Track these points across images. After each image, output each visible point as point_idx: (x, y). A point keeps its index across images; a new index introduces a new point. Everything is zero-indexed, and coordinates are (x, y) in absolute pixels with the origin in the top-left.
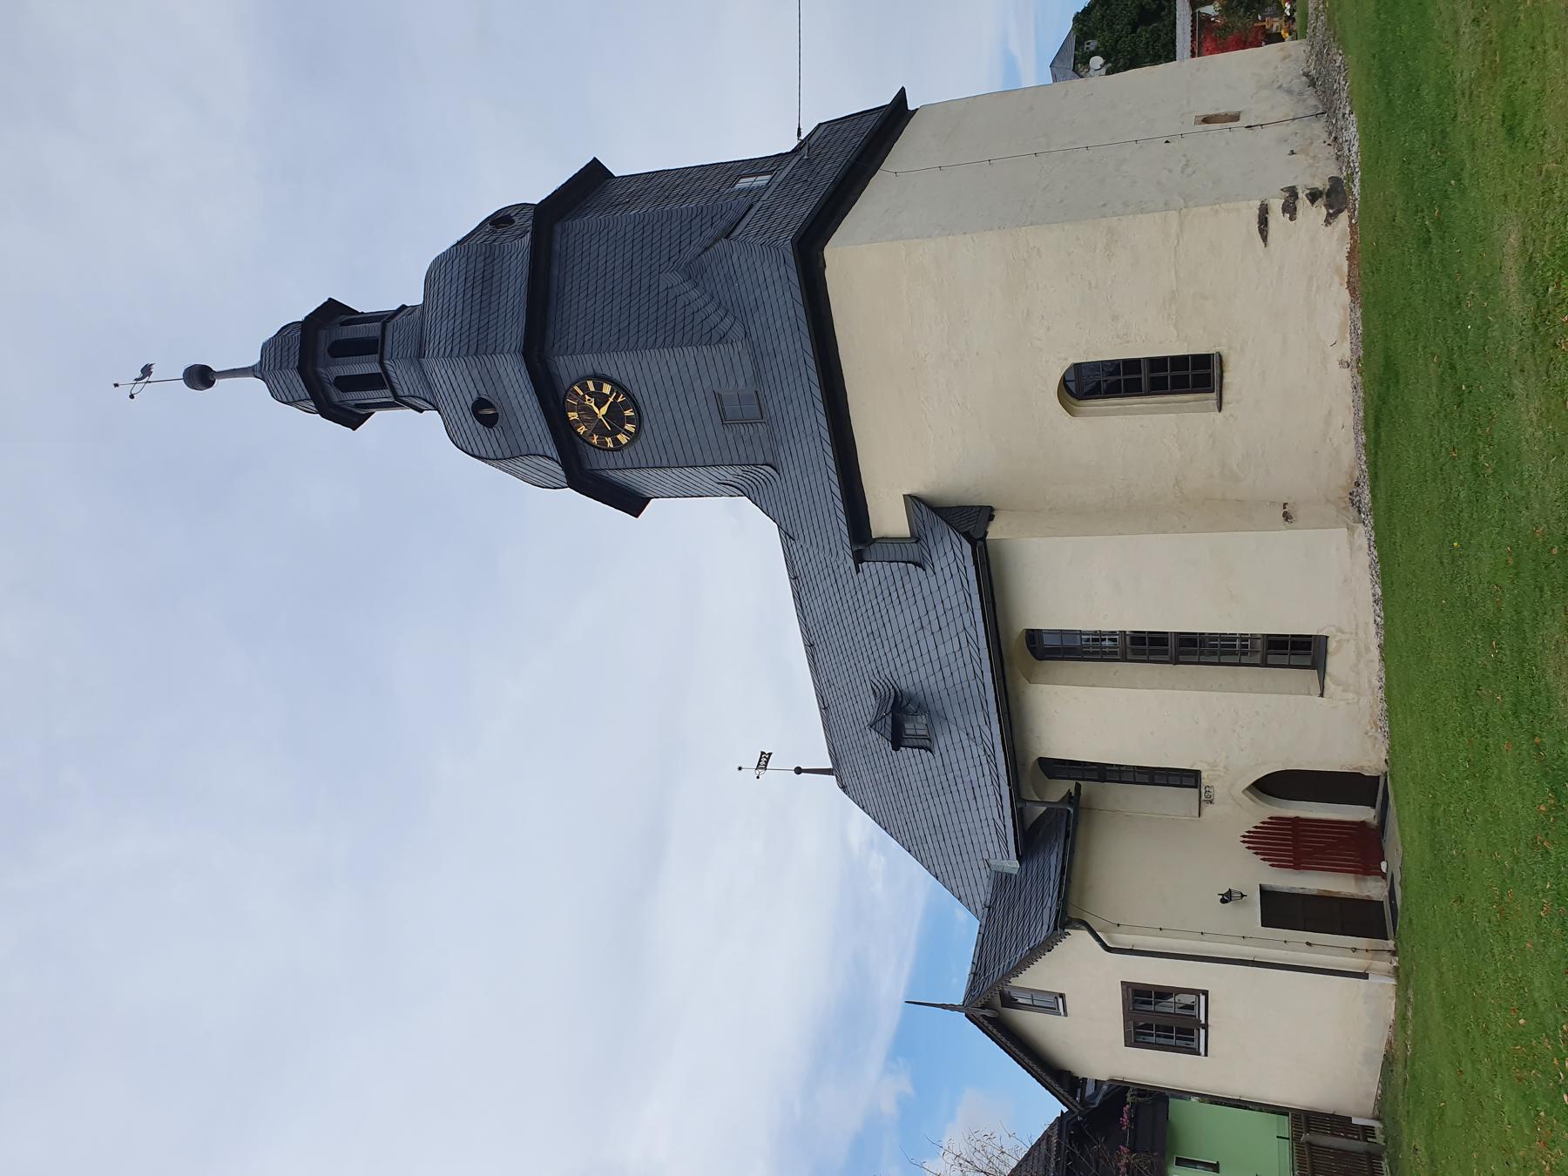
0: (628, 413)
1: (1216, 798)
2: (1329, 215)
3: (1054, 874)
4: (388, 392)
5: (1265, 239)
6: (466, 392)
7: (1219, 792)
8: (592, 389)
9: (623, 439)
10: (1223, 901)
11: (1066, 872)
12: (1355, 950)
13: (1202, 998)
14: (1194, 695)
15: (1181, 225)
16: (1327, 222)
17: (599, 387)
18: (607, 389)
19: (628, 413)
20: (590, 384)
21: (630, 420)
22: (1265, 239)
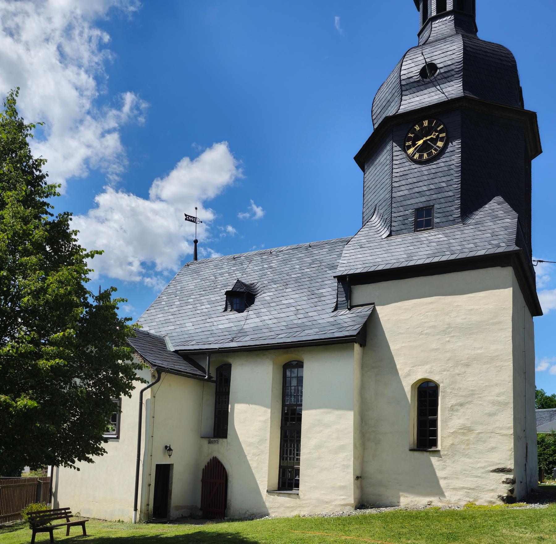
0: (425, 155)
1: (211, 445)
2: (503, 498)
3: (177, 367)
4: (434, 14)
5: (494, 471)
6: (442, 60)
7: (215, 447)
8: (441, 136)
9: (410, 151)
10: (166, 447)
11: (178, 373)
12: (148, 505)
13: (115, 436)
14: (351, 429)
15: (506, 435)
16: (499, 496)
17: (442, 139)
18: (440, 144)
19: (425, 155)
20: (407, 144)
21: (421, 156)
22: (494, 471)
